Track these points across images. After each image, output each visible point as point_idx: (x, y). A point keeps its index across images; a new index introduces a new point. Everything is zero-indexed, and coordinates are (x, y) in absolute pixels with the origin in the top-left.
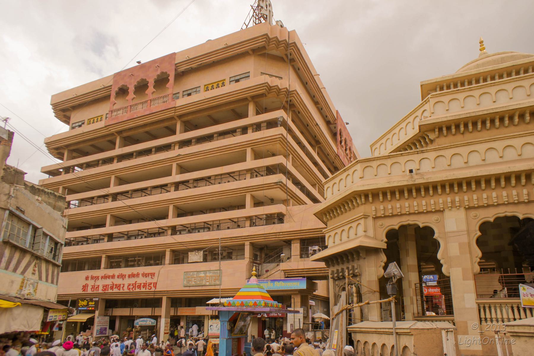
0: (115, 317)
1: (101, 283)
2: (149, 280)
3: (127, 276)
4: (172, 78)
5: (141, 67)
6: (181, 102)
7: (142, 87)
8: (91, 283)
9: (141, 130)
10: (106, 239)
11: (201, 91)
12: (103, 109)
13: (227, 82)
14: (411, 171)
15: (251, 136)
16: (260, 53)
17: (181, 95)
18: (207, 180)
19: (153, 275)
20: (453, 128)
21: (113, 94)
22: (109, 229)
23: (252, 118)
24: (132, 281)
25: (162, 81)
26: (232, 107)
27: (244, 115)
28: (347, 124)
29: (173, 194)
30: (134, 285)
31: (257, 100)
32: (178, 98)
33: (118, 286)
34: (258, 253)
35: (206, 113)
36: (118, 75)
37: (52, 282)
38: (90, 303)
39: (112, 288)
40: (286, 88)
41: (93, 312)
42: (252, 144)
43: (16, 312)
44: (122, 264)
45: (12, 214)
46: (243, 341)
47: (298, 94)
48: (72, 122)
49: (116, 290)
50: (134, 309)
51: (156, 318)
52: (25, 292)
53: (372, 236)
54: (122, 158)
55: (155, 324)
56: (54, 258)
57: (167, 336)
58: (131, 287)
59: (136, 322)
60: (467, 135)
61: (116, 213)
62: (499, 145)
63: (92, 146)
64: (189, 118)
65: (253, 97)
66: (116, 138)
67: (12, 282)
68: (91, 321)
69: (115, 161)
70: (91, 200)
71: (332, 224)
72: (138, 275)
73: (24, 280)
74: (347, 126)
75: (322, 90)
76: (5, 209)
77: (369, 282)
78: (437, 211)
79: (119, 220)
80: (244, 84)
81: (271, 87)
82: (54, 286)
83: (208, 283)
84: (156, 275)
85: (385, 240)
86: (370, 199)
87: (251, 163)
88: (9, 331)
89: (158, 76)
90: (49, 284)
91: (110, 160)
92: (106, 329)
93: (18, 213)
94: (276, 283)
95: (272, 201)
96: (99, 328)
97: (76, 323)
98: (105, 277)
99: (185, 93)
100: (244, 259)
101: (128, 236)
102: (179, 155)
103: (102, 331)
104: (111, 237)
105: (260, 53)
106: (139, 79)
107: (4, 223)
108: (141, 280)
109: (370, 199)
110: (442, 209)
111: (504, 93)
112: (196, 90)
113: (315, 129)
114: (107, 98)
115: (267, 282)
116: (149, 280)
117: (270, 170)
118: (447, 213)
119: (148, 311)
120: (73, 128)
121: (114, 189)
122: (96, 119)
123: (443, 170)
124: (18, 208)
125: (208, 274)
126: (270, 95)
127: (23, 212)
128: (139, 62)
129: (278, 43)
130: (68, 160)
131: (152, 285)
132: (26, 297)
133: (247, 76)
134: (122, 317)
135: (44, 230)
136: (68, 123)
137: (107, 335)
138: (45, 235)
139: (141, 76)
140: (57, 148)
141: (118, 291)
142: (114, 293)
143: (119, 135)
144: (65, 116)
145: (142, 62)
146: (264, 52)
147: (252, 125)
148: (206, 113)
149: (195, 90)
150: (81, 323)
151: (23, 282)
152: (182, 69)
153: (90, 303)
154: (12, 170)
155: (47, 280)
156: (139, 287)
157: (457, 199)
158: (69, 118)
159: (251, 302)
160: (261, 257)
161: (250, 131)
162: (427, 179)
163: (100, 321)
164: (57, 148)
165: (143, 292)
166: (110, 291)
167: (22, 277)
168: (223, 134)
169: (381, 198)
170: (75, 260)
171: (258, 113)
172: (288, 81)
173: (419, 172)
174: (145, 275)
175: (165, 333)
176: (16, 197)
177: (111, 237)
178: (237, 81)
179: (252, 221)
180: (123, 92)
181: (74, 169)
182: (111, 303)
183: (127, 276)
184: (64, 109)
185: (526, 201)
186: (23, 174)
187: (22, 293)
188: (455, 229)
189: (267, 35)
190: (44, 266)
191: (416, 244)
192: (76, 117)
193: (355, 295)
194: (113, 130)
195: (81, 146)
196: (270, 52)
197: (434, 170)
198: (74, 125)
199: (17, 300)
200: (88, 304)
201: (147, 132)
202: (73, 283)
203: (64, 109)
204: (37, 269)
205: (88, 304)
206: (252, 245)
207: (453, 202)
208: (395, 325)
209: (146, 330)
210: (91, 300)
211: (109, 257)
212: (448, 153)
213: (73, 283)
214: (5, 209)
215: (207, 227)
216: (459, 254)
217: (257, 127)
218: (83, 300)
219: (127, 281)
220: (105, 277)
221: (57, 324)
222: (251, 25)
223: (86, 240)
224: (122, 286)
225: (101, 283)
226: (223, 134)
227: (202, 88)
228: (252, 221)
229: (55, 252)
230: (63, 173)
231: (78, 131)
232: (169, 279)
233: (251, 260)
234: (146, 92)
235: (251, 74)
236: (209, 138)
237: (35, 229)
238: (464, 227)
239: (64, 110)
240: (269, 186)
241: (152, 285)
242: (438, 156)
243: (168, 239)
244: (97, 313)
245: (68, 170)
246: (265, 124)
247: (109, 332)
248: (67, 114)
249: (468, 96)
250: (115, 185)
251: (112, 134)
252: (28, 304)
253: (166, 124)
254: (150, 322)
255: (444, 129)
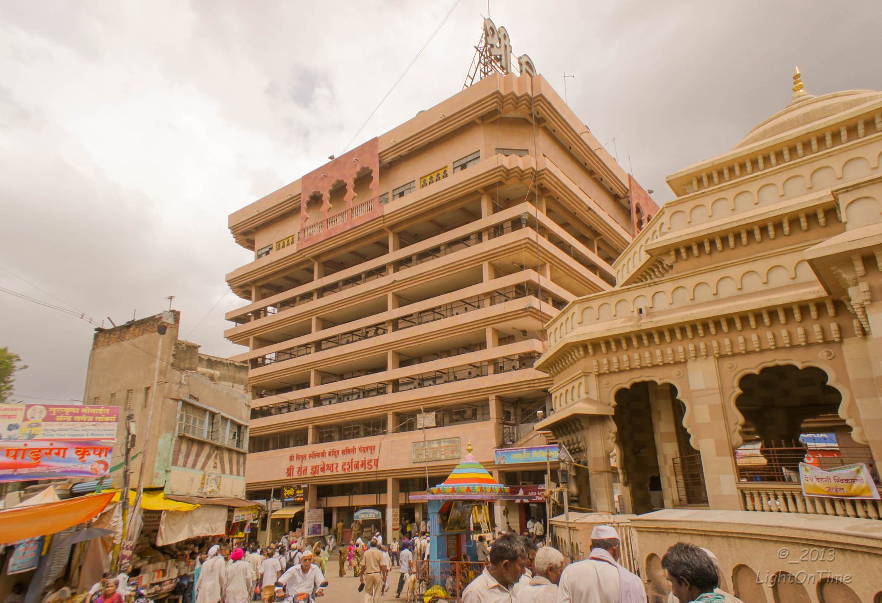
0: (332, 508)
1: (309, 463)
2: (368, 456)
3: (340, 453)
4: (376, 175)
5: (335, 163)
6: (393, 206)
7: (338, 191)
8: (296, 464)
9: (343, 252)
10: (312, 403)
11: (418, 188)
12: (292, 227)
13: (449, 170)
14: (640, 311)
15: (489, 244)
16: (491, 120)
17: (390, 196)
18: (434, 311)
19: (372, 448)
20: (695, 248)
21: (304, 205)
22: (315, 390)
23: (489, 219)
24: (347, 458)
25: (363, 180)
26: (459, 205)
27: (476, 215)
28: (651, 192)
29: (391, 337)
30: (350, 464)
31: (490, 191)
32: (387, 201)
33: (330, 467)
34: (512, 410)
35: (426, 218)
36: (306, 178)
37: (238, 474)
38: (298, 492)
39: (323, 470)
40: (532, 168)
41: (302, 503)
42: (488, 256)
43: (197, 514)
44: (336, 435)
45: (185, 404)
46: (464, 538)
47: (550, 172)
48: (257, 246)
49: (328, 473)
50: (354, 497)
51: (382, 508)
52: (207, 489)
53: (596, 399)
54: (322, 291)
55: (380, 517)
56: (238, 445)
57: (398, 534)
58: (347, 467)
59: (356, 514)
60: (716, 256)
61: (322, 367)
62: (761, 266)
63: (286, 278)
64: (404, 227)
65: (486, 189)
66: (313, 266)
67: (192, 480)
68: (300, 517)
69: (315, 296)
70: (290, 353)
71: (559, 381)
72: (354, 450)
73: (204, 476)
74: (651, 195)
75: (597, 152)
76: (177, 400)
77: (595, 459)
78: (677, 363)
79: (326, 376)
80: (474, 170)
81: (508, 170)
82: (241, 478)
83: (443, 457)
84: (377, 449)
85: (614, 403)
86: (590, 351)
87: (489, 284)
88: (191, 536)
89: (358, 173)
90: (234, 477)
91: (307, 296)
92: (320, 526)
93: (192, 401)
94: (534, 452)
95: (525, 334)
96: (311, 525)
97: (283, 520)
98: (314, 455)
99: (395, 193)
100: (489, 419)
101: (339, 397)
102: (395, 281)
103: (315, 530)
104: (318, 401)
105: (491, 120)
106: (334, 181)
107: (178, 416)
108: (358, 457)
109: (590, 351)
110: (683, 360)
111: (771, 189)
112: (409, 186)
113: (588, 217)
114: (296, 211)
115: (522, 452)
116: (368, 456)
117: (521, 290)
118: (690, 364)
119: (370, 499)
120: (259, 256)
121: (316, 335)
122: (286, 241)
123: (684, 307)
124: (191, 396)
125: (443, 444)
126: (509, 182)
127: (197, 399)
128: (331, 158)
129: (516, 100)
130: (257, 300)
131: (373, 463)
132: (209, 495)
133: (475, 157)
134: (340, 509)
135: (223, 414)
136: (252, 248)
137: (322, 535)
138: (225, 419)
139: (336, 176)
140: (243, 285)
141: (331, 474)
142: (326, 476)
143: (316, 260)
144: (248, 241)
145: (336, 156)
146: (498, 117)
147: (487, 229)
148: (426, 218)
149: (408, 186)
150: (290, 519)
151: (204, 479)
152: (388, 159)
153: (298, 492)
154: (184, 345)
155: (231, 473)
156: (357, 466)
157: (702, 346)
158: (253, 242)
159: (464, 486)
160: (515, 414)
161: (485, 237)
162: (657, 322)
163: (312, 516)
164: (243, 285)
165: (361, 474)
166: (321, 474)
167: (202, 473)
168: (452, 245)
169: (604, 349)
170: (276, 434)
171: (496, 209)
172: (540, 156)
173: (652, 310)
174: (363, 450)
175: (394, 530)
176: (188, 385)
177: (318, 401)
178: (463, 167)
179: (498, 366)
180: (316, 200)
181: (266, 312)
182: (324, 491)
183: (340, 453)
184: (247, 231)
185: (787, 345)
186: (195, 348)
187: (204, 490)
188: (703, 387)
189: (498, 92)
190: (226, 456)
191: (640, 411)
192: (262, 240)
193: (620, 471)
194: (308, 255)
195: (271, 280)
196: (507, 115)
197: (673, 307)
198: (260, 253)
199: (197, 500)
200: (295, 494)
201: (353, 252)
202: (272, 466)
203: (247, 231)
204: (218, 461)
205: (295, 494)
206: (500, 399)
207: (697, 349)
208: (567, 518)
209: (370, 526)
210: (299, 488)
211: (317, 428)
212: (690, 283)
213: (272, 466)
214: (177, 400)
215: (435, 378)
216: (709, 421)
217: (497, 230)
218: (289, 488)
219: (340, 460)
220: (314, 455)
221: (248, 524)
222: (477, 79)
223: (289, 407)
224: (335, 466)
225: (309, 463)
226: (452, 245)
227: (418, 184)
228: (498, 366)
229: (239, 436)
230: (252, 318)
231: (266, 260)
232: (393, 453)
233: (500, 421)
234: (345, 199)
235: (481, 154)
236: (435, 252)
237: (213, 415)
238: (714, 383)
239: (245, 234)
240: (516, 315)
241: (373, 463)
242: (678, 288)
243: (390, 398)
244: (307, 504)
245: (257, 314)
246: (509, 224)
247: (324, 530)
248: (250, 237)
249: (718, 200)
250: (318, 329)
251: (308, 261)
252: (209, 504)
253: (375, 239)
254: (373, 514)
255: (683, 251)
